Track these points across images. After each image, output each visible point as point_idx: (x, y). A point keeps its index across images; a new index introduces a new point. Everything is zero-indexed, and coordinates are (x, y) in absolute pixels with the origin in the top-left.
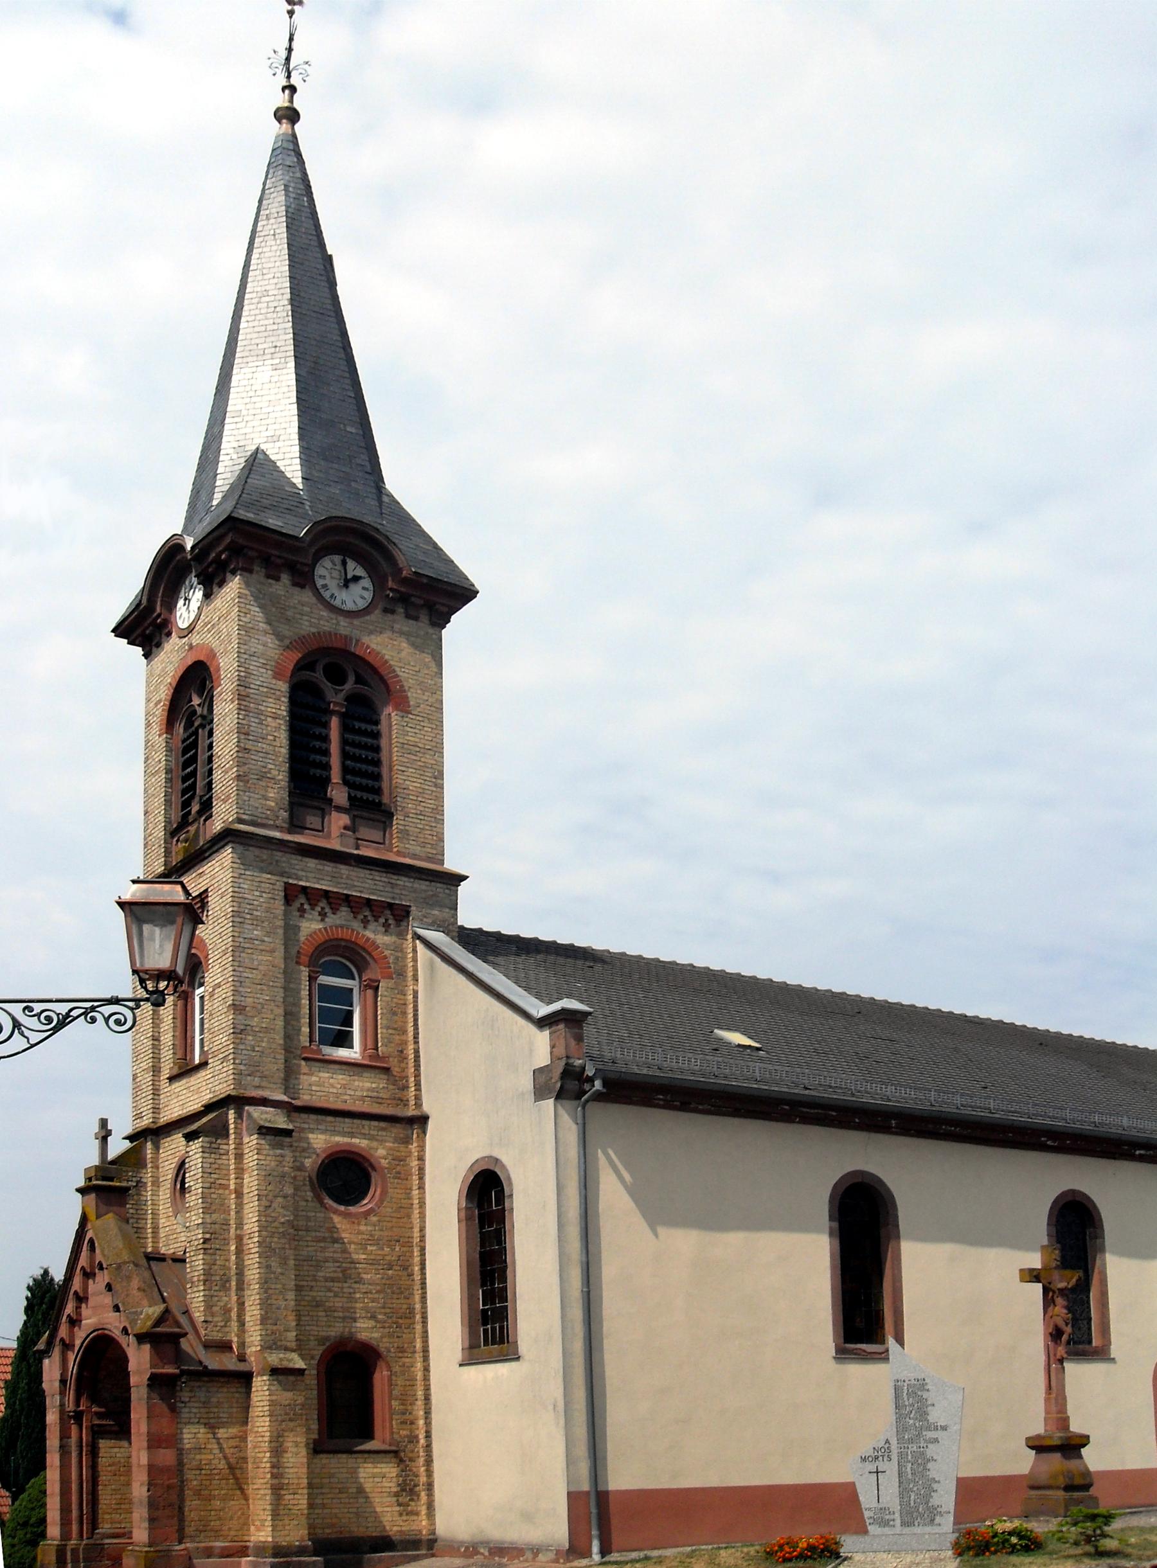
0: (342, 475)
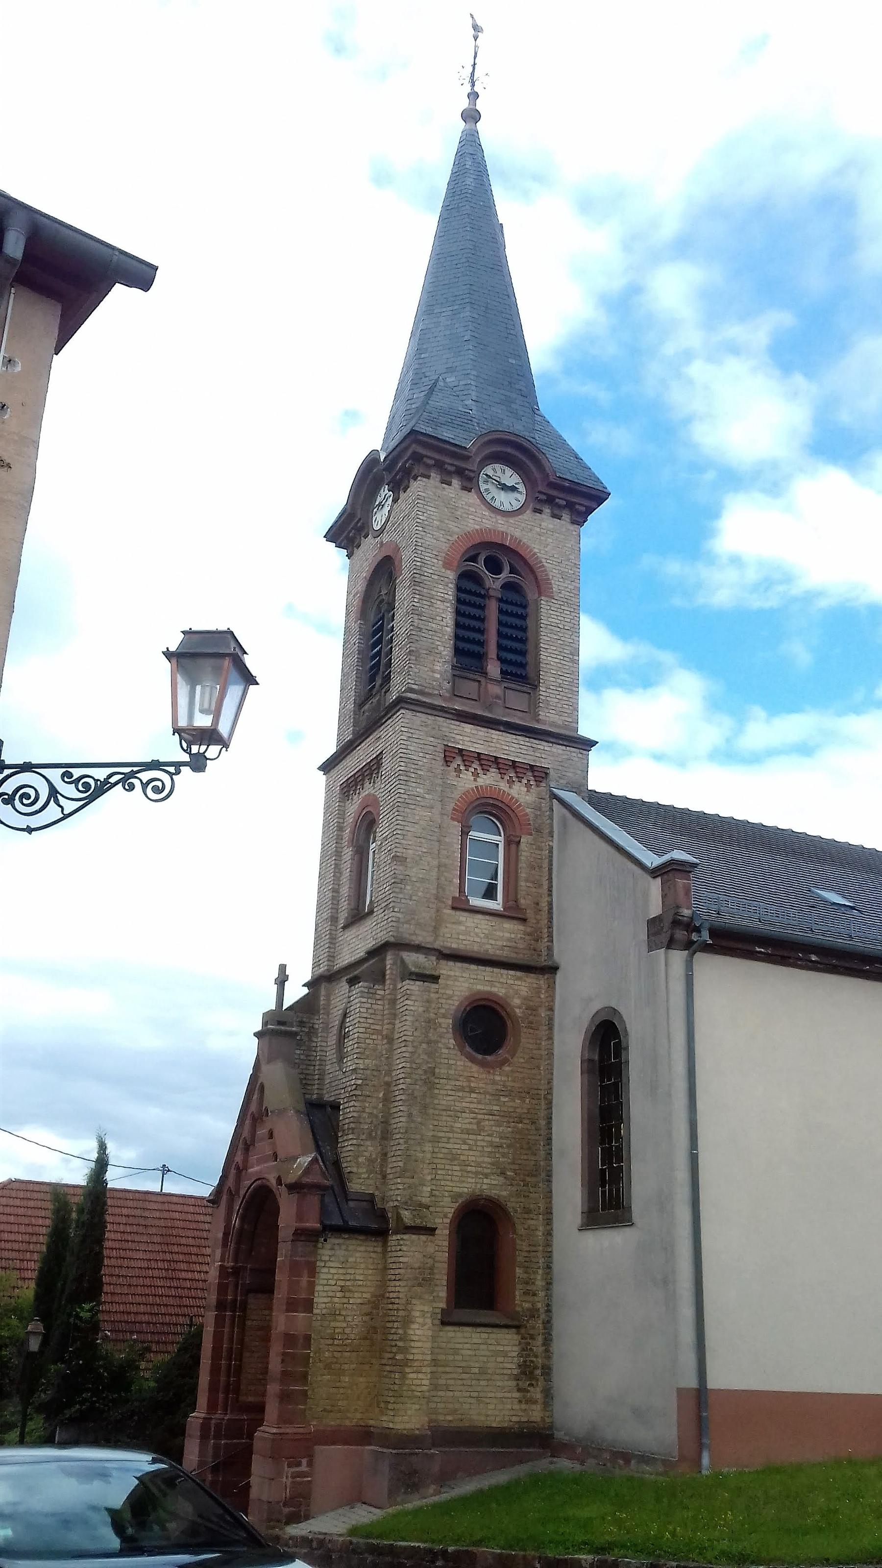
0: (503, 397)
